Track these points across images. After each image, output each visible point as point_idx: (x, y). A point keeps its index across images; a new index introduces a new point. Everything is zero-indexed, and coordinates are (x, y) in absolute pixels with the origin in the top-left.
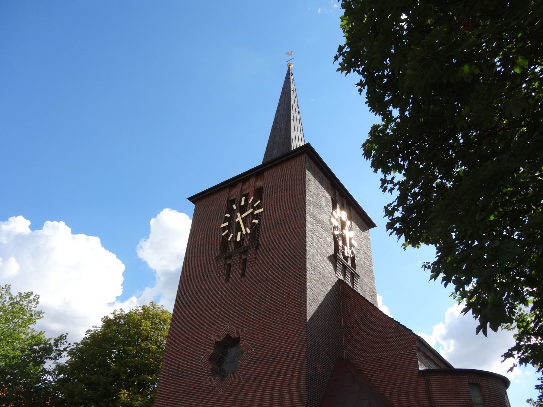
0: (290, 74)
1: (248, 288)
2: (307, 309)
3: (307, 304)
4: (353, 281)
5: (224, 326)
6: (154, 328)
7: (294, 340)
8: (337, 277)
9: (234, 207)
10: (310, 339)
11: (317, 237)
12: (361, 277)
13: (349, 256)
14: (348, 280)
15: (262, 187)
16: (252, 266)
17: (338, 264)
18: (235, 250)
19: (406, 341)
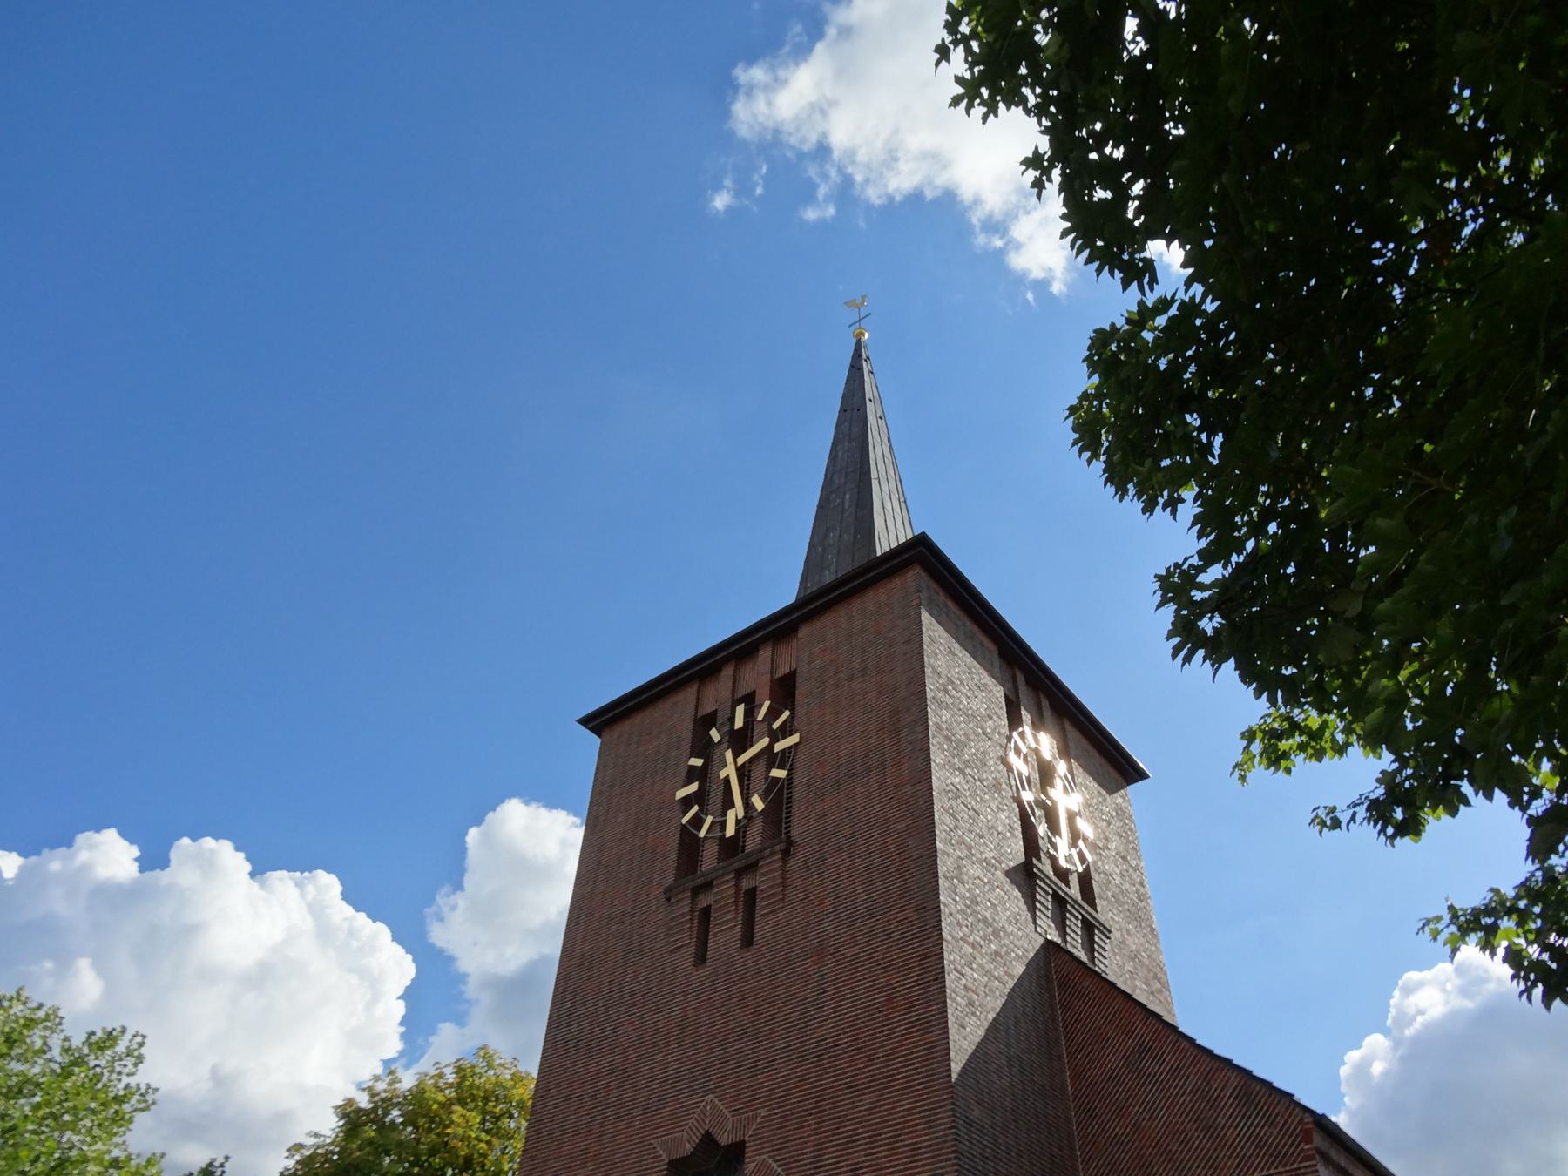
0: (860, 356)
1: (763, 979)
2: (951, 1037)
3: (949, 1022)
4: (1090, 945)
5: (693, 1108)
6: (487, 1132)
7: (916, 1143)
8: (1040, 934)
9: (715, 735)
10: (966, 1134)
11: (969, 809)
12: (1116, 935)
13: (1072, 868)
14: (1074, 943)
15: (795, 671)
16: (775, 910)
17: (1040, 894)
18: (721, 864)
19: (1278, 1133)
